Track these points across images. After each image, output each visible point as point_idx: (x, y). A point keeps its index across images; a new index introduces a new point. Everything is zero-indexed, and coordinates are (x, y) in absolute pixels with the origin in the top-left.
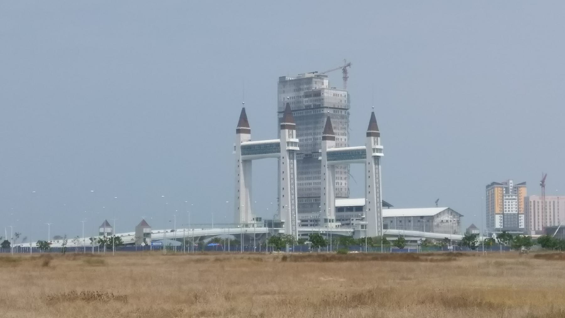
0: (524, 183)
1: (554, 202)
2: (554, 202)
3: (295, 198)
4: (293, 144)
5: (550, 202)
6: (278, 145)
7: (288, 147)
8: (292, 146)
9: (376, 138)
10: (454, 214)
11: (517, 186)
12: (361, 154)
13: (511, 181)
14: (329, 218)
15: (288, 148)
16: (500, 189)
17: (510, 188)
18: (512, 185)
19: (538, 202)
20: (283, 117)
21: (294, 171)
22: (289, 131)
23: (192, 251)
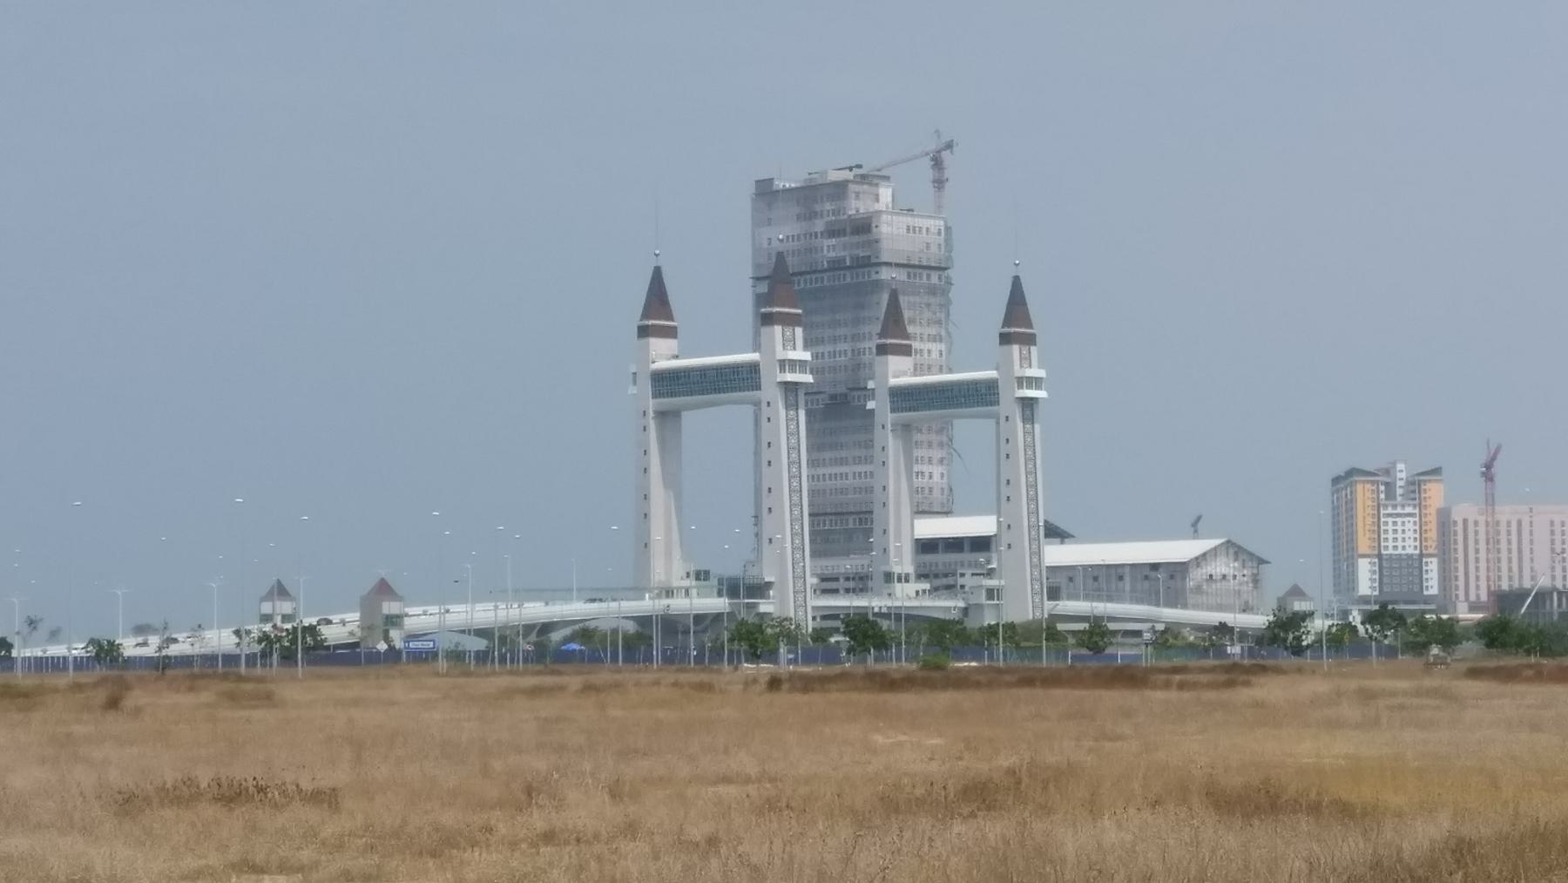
0: (1436, 471)
1: (1519, 523)
2: (1519, 523)
6: (753, 368)
13: (1400, 466)
16: (1368, 486)
17: (1400, 483)
18: (1403, 475)
19: (1476, 523)
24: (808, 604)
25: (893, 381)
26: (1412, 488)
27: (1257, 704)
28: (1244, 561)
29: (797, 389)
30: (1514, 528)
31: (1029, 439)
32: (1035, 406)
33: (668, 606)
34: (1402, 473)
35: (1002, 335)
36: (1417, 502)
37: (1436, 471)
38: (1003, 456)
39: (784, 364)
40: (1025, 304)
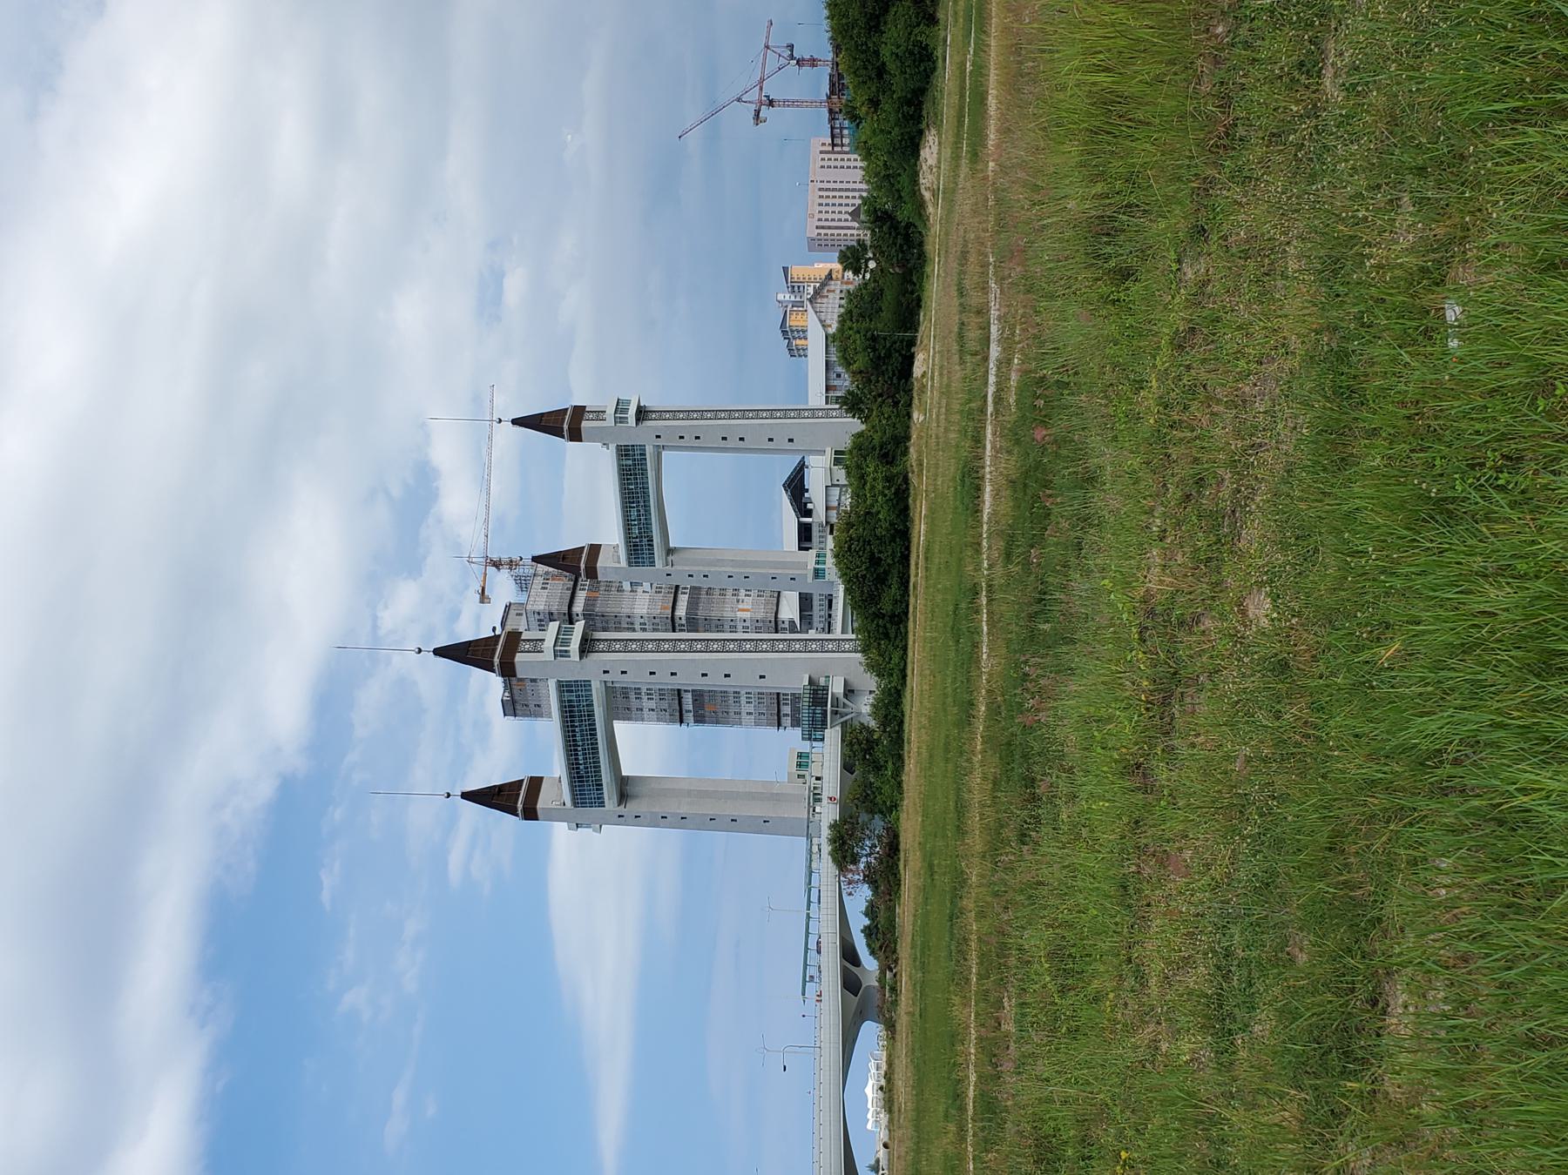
0: (785, 270)
1: (820, 190)
2: (820, 190)
3: (737, 640)
4: (561, 641)
5: (821, 197)
6: (564, 687)
7: (571, 654)
8: (566, 643)
9: (586, 415)
10: (825, 291)
11: (789, 284)
12: (630, 462)
13: (781, 297)
14: (811, 565)
15: (575, 655)
16: (793, 317)
17: (793, 298)
18: (787, 296)
19: (820, 220)
20: (623, 774)
21: (651, 640)
22: (522, 652)
23: (1418, 869)
24: (838, 638)
25: (624, 563)
26: (796, 289)
27: (982, 67)
28: (828, 291)
29: (591, 640)
30: (825, 194)
31: (797, 646)
32: (647, 409)
33: (831, 799)
34: (786, 296)
35: (572, 439)
36: (806, 284)
37: (785, 270)
38: (697, 443)
39: (560, 653)
40: (542, 415)
